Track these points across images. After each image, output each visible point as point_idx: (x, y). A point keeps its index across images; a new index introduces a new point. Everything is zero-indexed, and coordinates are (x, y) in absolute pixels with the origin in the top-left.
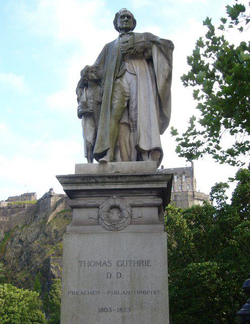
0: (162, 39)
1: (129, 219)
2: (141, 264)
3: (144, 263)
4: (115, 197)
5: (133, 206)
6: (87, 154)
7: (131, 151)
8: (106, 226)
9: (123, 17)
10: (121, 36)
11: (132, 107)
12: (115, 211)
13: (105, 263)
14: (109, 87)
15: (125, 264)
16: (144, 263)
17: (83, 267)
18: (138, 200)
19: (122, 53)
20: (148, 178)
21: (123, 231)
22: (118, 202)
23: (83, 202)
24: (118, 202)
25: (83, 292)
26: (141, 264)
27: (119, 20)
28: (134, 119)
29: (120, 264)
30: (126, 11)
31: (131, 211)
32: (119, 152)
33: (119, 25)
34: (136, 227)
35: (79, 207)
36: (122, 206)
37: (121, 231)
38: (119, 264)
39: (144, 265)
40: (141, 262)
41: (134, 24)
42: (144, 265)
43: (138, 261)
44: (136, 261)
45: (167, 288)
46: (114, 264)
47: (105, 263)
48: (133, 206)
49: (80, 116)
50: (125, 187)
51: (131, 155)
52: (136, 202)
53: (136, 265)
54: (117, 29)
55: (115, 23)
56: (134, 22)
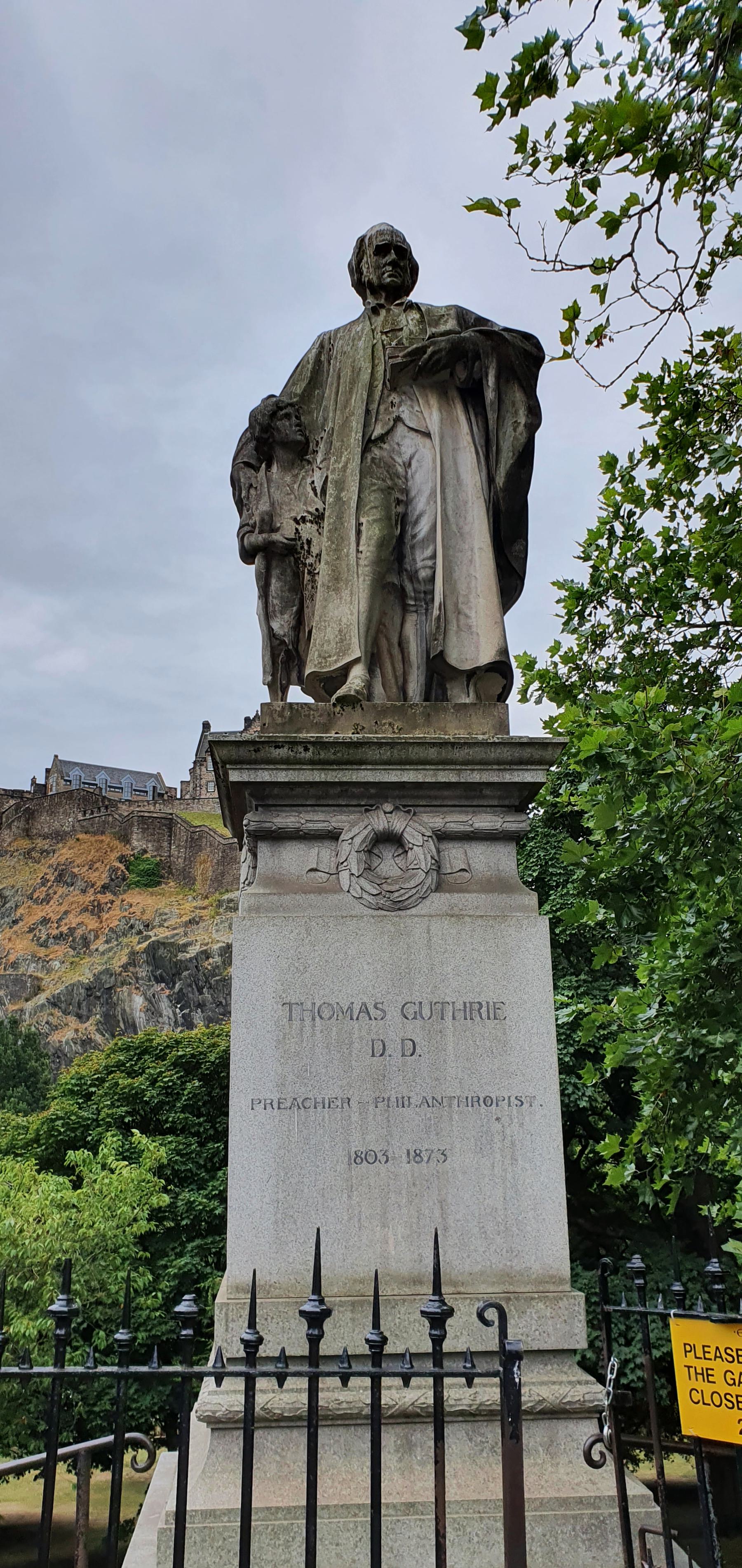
0: (506, 330)
1: (435, 874)
2: (475, 1014)
3: (484, 1009)
4: (388, 807)
5: (442, 837)
6: (273, 675)
7: (405, 675)
8: (365, 896)
9: (381, 250)
10: (375, 311)
11: (414, 536)
12: (388, 853)
13: (365, 1009)
14: (431, 414)
15: (426, 1012)
16: (484, 1009)
17: (296, 1024)
18: (456, 821)
19: (391, 361)
20: (459, 754)
21: (413, 911)
22: (398, 823)
23: (293, 819)
24: (398, 823)
25: (300, 1100)
26: (475, 1014)
27: (369, 260)
28: (423, 574)
29: (411, 1010)
30: (394, 233)
31: (438, 852)
32: (378, 670)
33: (369, 274)
34: (455, 898)
35: (278, 837)
36: (412, 836)
37: (408, 912)
38: (411, 1010)
39: (484, 1015)
40: (476, 1006)
41: (412, 276)
42: (484, 1015)
43: (465, 1003)
44: (459, 1006)
45: (236, 1015)
46: (393, 1013)
47: (365, 1009)
48: (442, 837)
49: (247, 555)
50: (318, 776)
51: (405, 682)
52: (452, 825)
53: (460, 1015)
54: (361, 286)
55: (355, 269)
56: (414, 270)
